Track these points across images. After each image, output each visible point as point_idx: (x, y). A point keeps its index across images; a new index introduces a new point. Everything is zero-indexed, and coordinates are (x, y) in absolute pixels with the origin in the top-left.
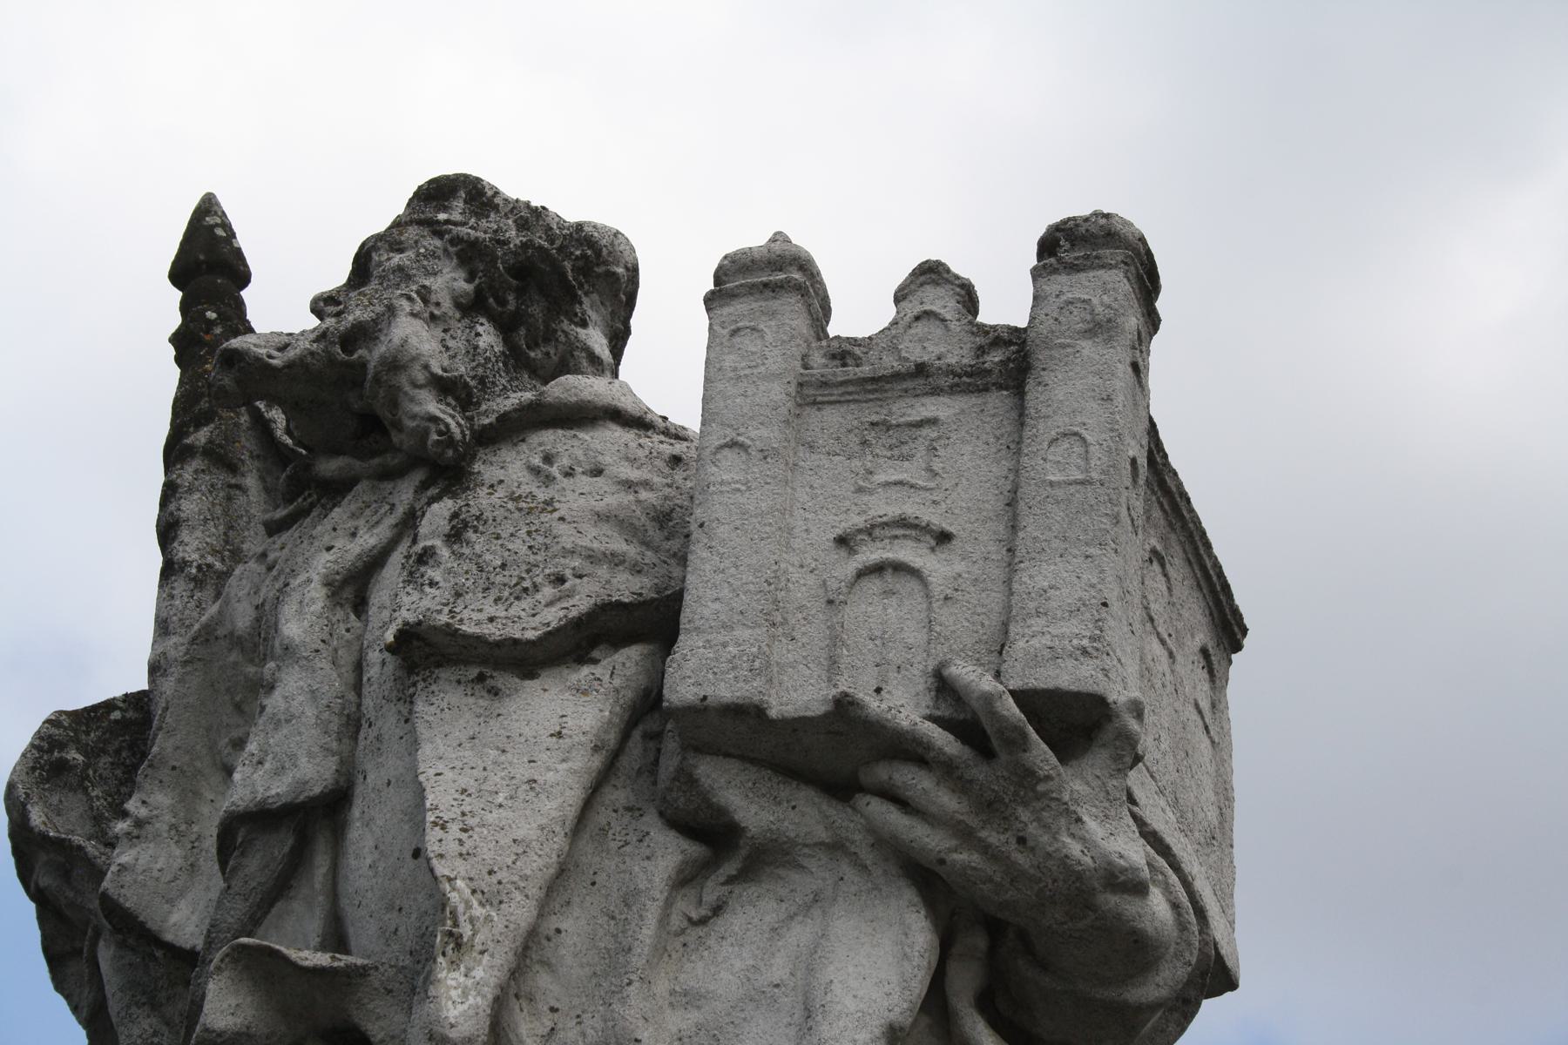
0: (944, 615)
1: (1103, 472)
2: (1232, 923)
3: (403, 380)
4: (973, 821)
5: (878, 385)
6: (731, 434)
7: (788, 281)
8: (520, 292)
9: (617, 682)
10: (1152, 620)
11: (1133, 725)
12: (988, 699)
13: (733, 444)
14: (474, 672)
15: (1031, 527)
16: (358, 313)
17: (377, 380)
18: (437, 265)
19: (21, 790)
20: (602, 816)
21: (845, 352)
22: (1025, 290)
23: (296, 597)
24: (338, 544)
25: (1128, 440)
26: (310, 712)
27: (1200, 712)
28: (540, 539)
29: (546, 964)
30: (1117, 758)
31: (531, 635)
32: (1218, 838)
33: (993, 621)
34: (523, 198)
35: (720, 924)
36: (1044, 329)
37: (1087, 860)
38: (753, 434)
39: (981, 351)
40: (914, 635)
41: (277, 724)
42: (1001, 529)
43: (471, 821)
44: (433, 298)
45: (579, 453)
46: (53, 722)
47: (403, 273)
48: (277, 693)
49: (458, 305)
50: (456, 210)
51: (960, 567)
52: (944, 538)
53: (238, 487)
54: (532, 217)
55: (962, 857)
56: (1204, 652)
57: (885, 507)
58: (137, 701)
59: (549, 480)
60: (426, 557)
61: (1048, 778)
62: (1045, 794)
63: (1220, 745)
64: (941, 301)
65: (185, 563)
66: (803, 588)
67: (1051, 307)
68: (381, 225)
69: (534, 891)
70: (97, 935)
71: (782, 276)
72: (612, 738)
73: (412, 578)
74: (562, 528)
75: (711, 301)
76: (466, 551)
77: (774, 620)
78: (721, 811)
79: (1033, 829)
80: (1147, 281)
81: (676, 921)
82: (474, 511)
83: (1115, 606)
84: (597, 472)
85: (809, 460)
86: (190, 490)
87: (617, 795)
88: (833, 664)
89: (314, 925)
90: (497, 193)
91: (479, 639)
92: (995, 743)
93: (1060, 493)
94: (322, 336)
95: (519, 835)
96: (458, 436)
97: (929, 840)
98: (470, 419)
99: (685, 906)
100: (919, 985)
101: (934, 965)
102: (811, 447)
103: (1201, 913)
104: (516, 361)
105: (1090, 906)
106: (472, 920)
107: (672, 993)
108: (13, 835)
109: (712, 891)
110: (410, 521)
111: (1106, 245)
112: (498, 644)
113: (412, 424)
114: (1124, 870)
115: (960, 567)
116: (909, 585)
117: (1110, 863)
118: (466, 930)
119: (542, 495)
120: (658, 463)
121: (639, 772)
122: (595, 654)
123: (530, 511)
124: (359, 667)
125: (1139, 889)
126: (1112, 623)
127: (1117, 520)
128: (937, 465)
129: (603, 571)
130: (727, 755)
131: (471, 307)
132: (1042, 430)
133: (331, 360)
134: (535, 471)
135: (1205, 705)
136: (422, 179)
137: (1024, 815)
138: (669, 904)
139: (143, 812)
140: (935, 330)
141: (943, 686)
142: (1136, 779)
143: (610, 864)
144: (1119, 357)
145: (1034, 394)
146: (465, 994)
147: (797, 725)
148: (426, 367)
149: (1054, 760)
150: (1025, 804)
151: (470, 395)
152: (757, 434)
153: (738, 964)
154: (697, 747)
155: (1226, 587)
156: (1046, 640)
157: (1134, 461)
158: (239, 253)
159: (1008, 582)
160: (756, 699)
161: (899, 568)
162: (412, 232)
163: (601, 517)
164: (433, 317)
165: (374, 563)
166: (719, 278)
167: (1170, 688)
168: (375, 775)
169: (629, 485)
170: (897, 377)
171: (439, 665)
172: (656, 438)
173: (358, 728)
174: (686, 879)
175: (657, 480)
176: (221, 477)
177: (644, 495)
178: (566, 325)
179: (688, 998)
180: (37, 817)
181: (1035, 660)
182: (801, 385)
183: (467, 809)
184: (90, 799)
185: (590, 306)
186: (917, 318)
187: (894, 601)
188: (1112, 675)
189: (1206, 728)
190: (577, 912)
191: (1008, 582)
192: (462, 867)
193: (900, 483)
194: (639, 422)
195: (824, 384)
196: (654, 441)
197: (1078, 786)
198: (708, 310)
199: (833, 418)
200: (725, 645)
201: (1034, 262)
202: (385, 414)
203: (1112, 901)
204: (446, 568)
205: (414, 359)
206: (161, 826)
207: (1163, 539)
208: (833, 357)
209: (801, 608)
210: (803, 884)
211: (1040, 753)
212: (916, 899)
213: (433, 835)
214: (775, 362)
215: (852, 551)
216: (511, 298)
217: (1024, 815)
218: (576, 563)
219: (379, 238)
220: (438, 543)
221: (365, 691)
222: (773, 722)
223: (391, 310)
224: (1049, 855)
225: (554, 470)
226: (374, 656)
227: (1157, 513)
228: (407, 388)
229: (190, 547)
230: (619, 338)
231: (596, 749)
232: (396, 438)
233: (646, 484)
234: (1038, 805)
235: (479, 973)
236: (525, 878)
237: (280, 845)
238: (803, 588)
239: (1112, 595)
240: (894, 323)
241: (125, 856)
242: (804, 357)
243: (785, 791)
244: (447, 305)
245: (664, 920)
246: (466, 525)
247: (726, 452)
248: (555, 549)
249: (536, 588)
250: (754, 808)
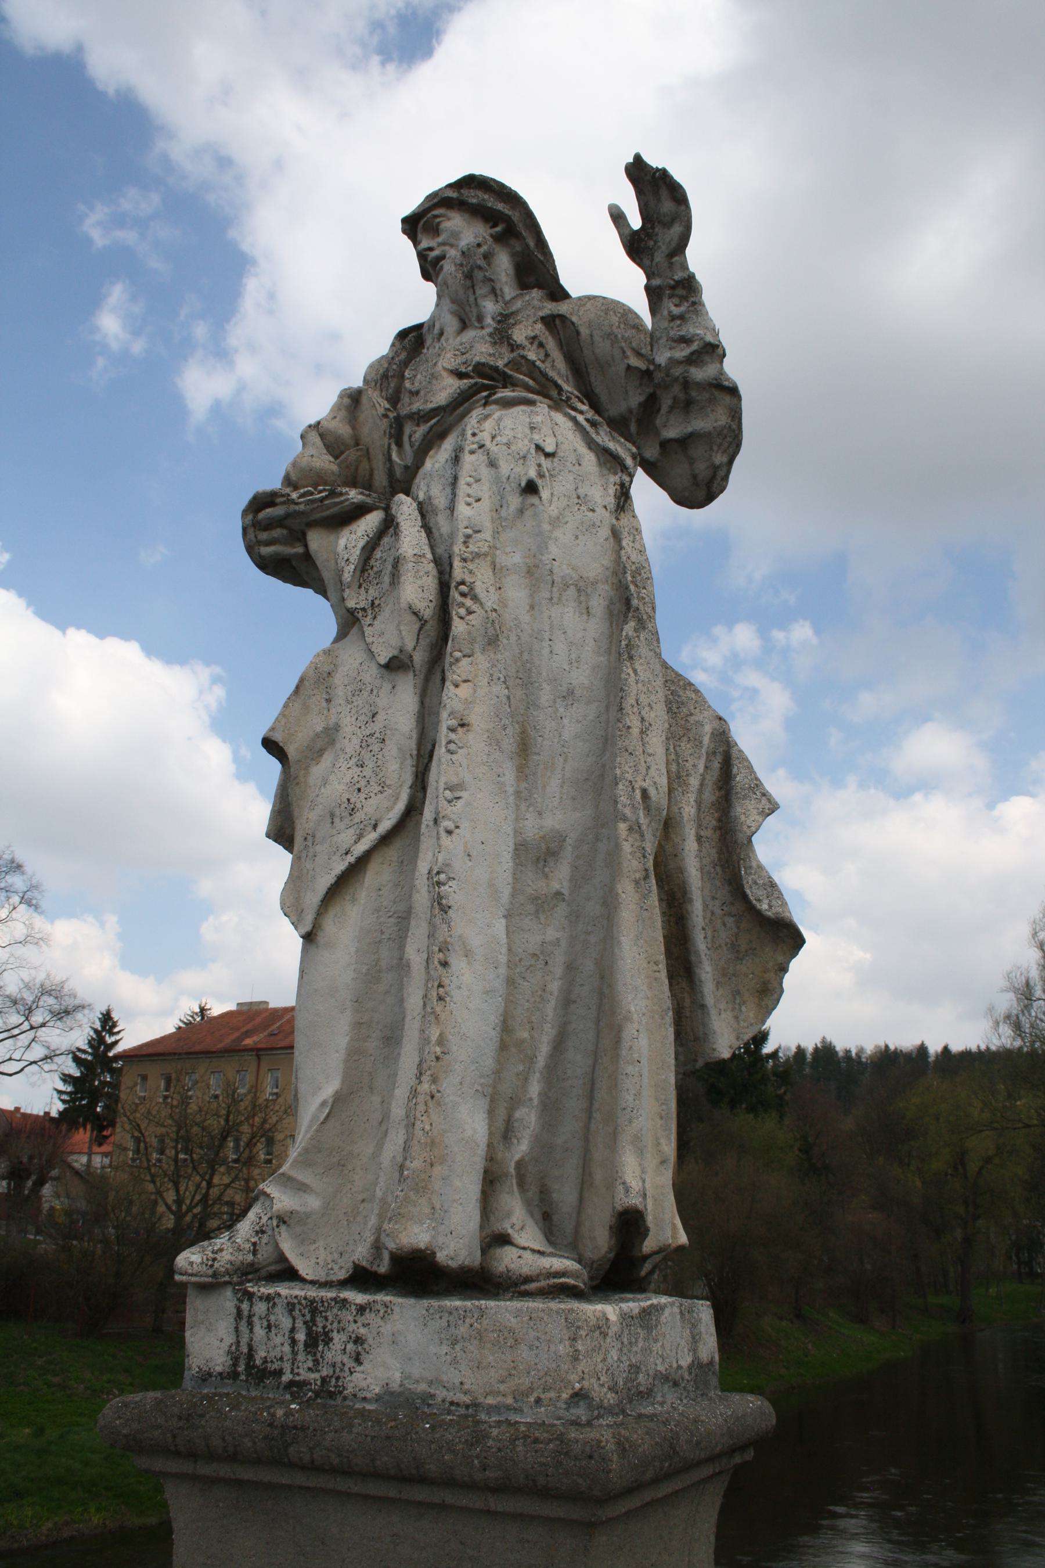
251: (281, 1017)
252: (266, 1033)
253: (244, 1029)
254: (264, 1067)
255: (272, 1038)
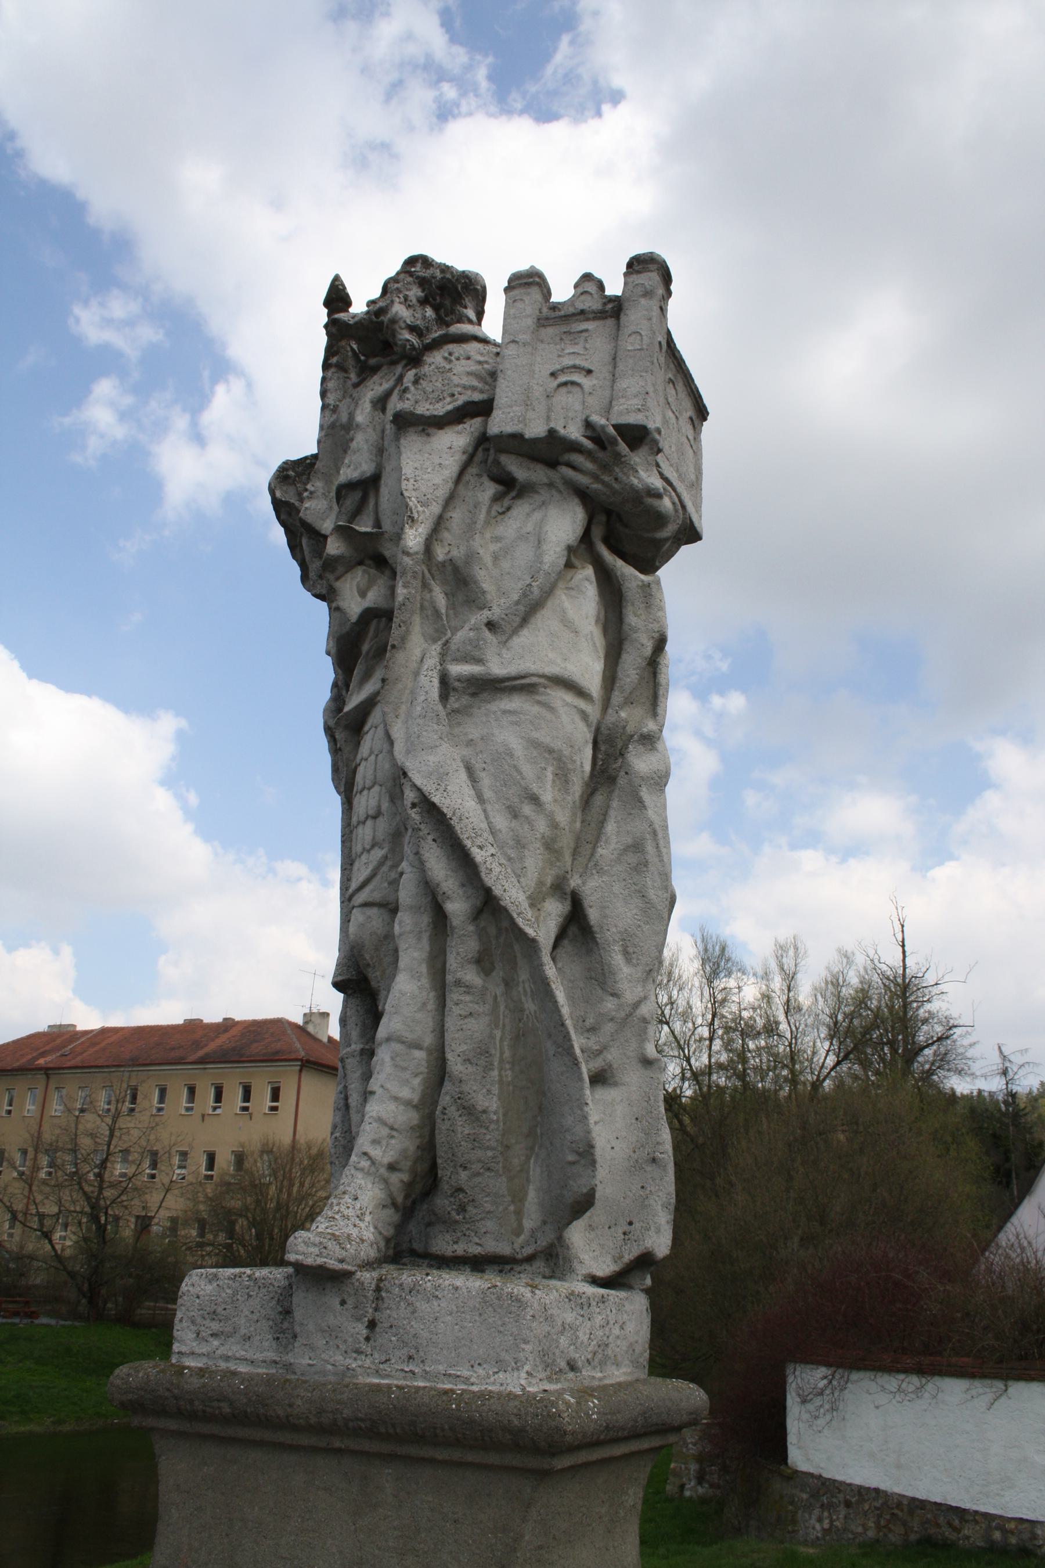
0: (590, 400)
1: (648, 345)
2: (700, 517)
3: (397, 327)
4: (599, 473)
5: (567, 318)
6: (512, 338)
7: (534, 281)
8: (442, 296)
9: (472, 429)
10: (669, 404)
11: (657, 437)
12: (603, 427)
13: (513, 341)
14: (421, 428)
15: (621, 366)
16: (381, 304)
17: (387, 327)
18: (410, 287)
19: (273, 485)
20: (467, 477)
21: (555, 307)
22: (621, 280)
23: (360, 407)
24: (376, 388)
25: (657, 334)
26: (365, 447)
27: (689, 440)
28: (446, 382)
29: (447, 529)
30: (651, 449)
31: (441, 414)
32: (696, 485)
33: (608, 400)
34: (443, 262)
35: (509, 514)
36: (627, 295)
37: (640, 486)
38: (520, 337)
39: (605, 304)
40: (578, 407)
41: (355, 453)
42: (610, 368)
43: (418, 478)
44: (409, 299)
45: (462, 352)
46: (286, 463)
47: (398, 290)
48: (354, 442)
49: (419, 301)
50: (418, 268)
51: (595, 382)
52: (589, 372)
53: (348, 378)
54: (445, 269)
55: (596, 486)
56: (691, 419)
57: (568, 361)
58: (315, 457)
59: (450, 361)
60: (406, 390)
61: (625, 456)
62: (625, 462)
63: (697, 453)
64: (591, 287)
65: (329, 405)
66: (538, 392)
67: (630, 287)
68: (392, 274)
69: (441, 502)
70: (302, 535)
71: (531, 280)
72: (470, 449)
73: (401, 398)
74: (454, 377)
75: (507, 290)
76: (420, 387)
77: (527, 403)
78: (509, 474)
79: (620, 475)
80: (667, 278)
81: (493, 513)
82: (423, 373)
83: (651, 394)
84: (468, 358)
85: (540, 346)
86: (331, 379)
87: (473, 470)
88: (548, 418)
89: (371, 523)
90: (433, 260)
91: (422, 416)
92: (606, 443)
93: (631, 354)
94: (368, 313)
95: (436, 482)
96: (417, 346)
97: (583, 480)
98: (422, 341)
99: (497, 508)
100: (579, 531)
101: (585, 525)
102: (542, 341)
103: (684, 507)
104: (442, 321)
105: (641, 503)
106: (418, 512)
107: (492, 537)
108: (273, 503)
109: (506, 502)
110: (400, 379)
111: (650, 264)
112: (430, 417)
113: (400, 343)
114: (653, 489)
115: (595, 382)
116: (575, 389)
117: (649, 486)
118: (416, 515)
119: (448, 367)
120: (491, 355)
121: (481, 462)
122: (465, 420)
123: (443, 372)
124: (383, 431)
125: (659, 496)
126: (649, 399)
127: (653, 363)
128: (588, 346)
129: (469, 392)
130: (511, 453)
131: (423, 302)
132: (626, 331)
133: (371, 321)
134: (445, 358)
135: (691, 438)
136: (406, 257)
137: (617, 469)
138: (490, 507)
139: (313, 489)
140: (589, 297)
141: (588, 425)
142: (660, 458)
143: (470, 494)
144: (654, 304)
145: (623, 318)
146: (415, 537)
147: (535, 441)
148: (405, 322)
149: (627, 449)
150: (617, 466)
151: (422, 332)
152: (521, 337)
153: (515, 526)
154: (501, 451)
155: (700, 396)
156: (625, 406)
157: (660, 343)
158: (347, 295)
159: (612, 387)
160: (520, 431)
161: (573, 383)
162: (402, 276)
163: (469, 374)
164: (409, 306)
165: (388, 394)
166: (510, 281)
167: (676, 429)
168: (388, 468)
169: (480, 363)
170: (574, 315)
171: (409, 426)
172: (491, 346)
173: (383, 452)
174: (497, 498)
175: (491, 361)
176: (342, 375)
177: (486, 366)
178: (458, 307)
179: (497, 539)
180: (278, 494)
181: (621, 413)
182: (539, 319)
183: (416, 474)
184: (297, 488)
185: (467, 301)
186: (582, 294)
187: (571, 395)
188: (650, 418)
189: (691, 446)
190: (458, 510)
191: (612, 387)
192: (414, 494)
193: (574, 353)
194: (485, 341)
195: (547, 319)
196: (490, 348)
197: (637, 459)
198: (505, 293)
199: (550, 331)
200: (509, 413)
201: (625, 270)
202: (391, 340)
203: (650, 501)
204: (413, 393)
205: (401, 318)
206: (319, 494)
207: (675, 376)
208: (551, 309)
209: (537, 399)
210: (538, 499)
211: (623, 447)
212: (579, 502)
213: (404, 483)
214: (529, 310)
215: (556, 378)
216: (438, 298)
217: (617, 469)
218: (459, 389)
219: (391, 279)
220: (410, 385)
221: (385, 438)
222: (527, 440)
223: (392, 302)
224: (626, 484)
225: (453, 358)
226: (388, 426)
227: (672, 366)
228: (398, 330)
229: (331, 399)
230: (480, 314)
231: (464, 453)
232: (395, 349)
233: (486, 362)
234: (622, 466)
235: (420, 530)
236: (437, 497)
237: (357, 495)
238: (538, 392)
239: (650, 390)
240: (574, 296)
241: (307, 505)
242: (540, 309)
243: (532, 466)
244: (414, 301)
245: (489, 512)
246: (420, 378)
247: (511, 344)
248: (452, 385)
249: (444, 398)
250: (521, 472)
251: (78, 1039)
252: (58, 1054)
253: (42, 1050)
254: (52, 1085)
255: (64, 1057)
